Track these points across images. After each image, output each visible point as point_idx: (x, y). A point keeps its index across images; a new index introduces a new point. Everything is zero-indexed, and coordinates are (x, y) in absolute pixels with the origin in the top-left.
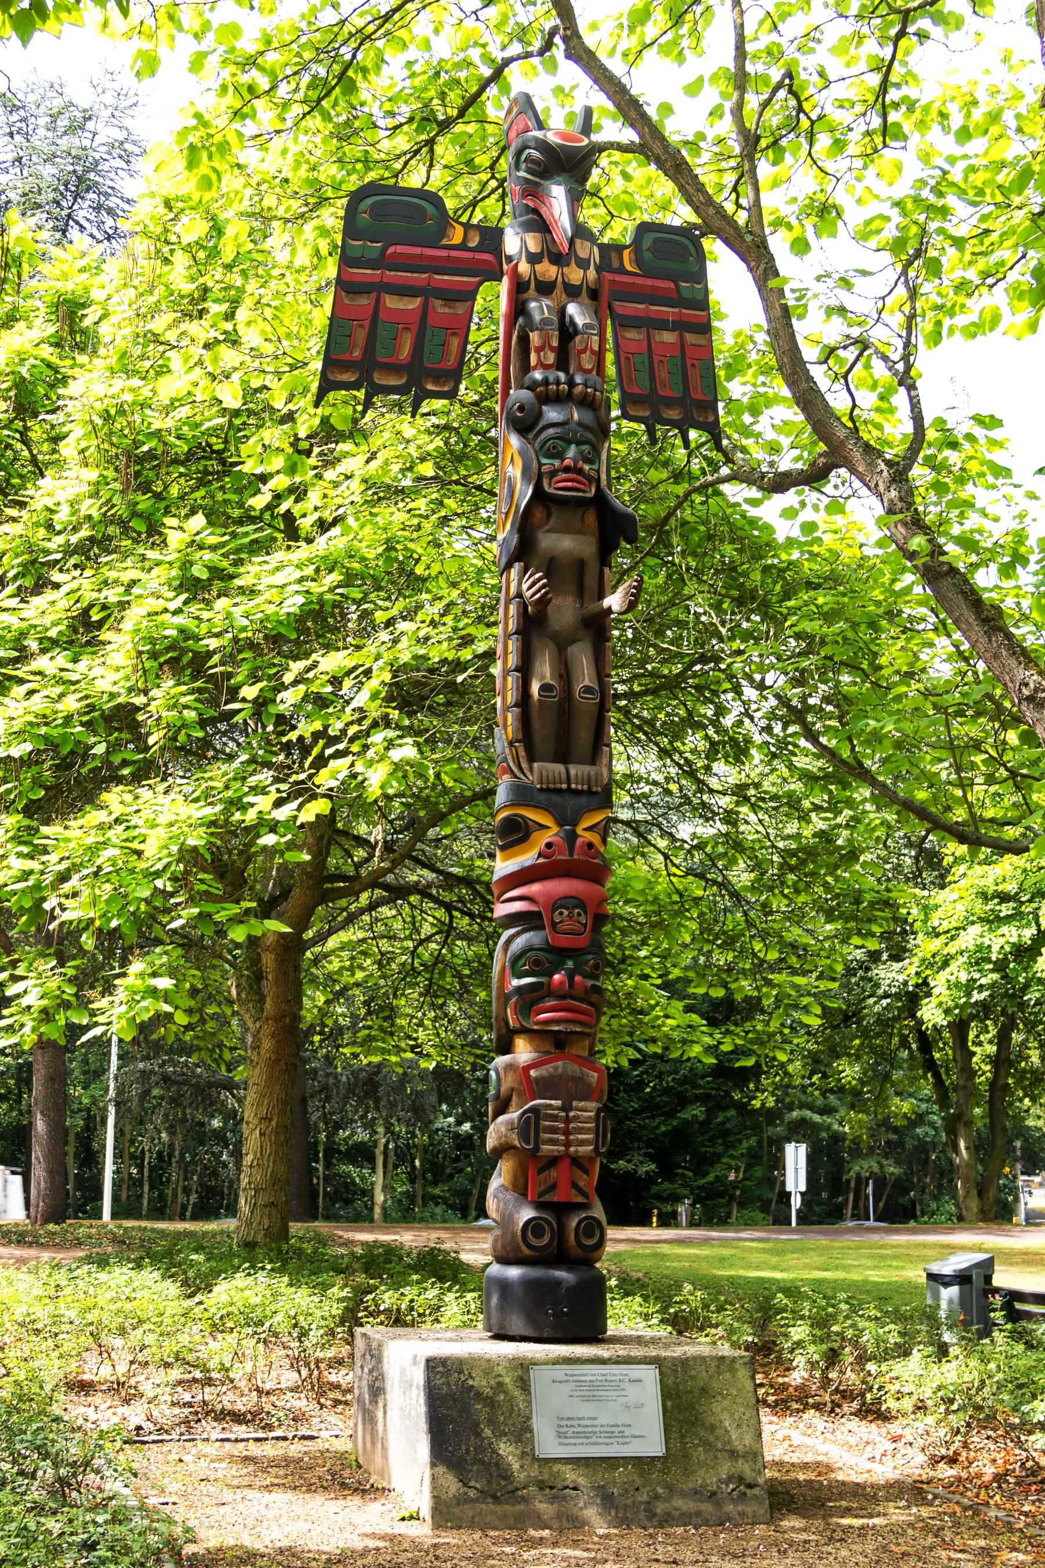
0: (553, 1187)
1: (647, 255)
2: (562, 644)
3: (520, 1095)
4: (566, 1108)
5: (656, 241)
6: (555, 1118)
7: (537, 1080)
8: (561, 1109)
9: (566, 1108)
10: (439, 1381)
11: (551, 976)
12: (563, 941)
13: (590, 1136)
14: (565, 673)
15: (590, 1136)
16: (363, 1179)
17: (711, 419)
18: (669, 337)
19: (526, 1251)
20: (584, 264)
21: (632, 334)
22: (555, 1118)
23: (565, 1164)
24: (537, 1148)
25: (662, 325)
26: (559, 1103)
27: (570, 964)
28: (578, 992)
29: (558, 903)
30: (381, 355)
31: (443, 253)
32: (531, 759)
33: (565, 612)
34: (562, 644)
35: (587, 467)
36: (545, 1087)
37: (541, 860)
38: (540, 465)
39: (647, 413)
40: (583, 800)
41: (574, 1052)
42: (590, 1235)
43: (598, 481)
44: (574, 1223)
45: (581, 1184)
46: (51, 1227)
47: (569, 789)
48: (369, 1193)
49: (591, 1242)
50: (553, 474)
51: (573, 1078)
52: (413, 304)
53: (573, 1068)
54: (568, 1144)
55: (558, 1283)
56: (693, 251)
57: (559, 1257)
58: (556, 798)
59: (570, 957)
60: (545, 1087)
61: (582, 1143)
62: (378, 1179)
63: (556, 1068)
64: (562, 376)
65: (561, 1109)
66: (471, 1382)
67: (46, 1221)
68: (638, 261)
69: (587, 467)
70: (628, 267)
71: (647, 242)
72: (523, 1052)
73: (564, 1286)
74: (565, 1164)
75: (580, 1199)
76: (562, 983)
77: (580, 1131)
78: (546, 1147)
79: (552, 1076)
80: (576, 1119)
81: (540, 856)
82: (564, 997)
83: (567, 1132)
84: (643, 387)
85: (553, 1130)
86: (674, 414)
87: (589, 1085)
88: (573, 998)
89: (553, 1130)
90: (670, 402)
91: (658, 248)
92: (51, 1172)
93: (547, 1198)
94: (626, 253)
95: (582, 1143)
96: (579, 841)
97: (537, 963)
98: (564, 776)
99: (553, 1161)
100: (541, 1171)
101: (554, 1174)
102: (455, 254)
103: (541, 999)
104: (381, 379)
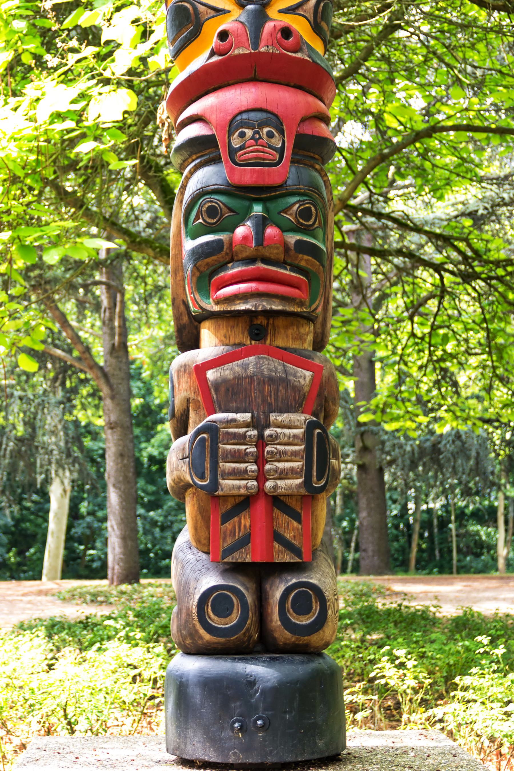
0: (244, 542)
3: (197, 408)
4: (259, 424)
6: (241, 439)
7: (217, 385)
8: (253, 424)
9: (259, 424)
11: (233, 231)
12: (247, 176)
13: (297, 465)
15: (297, 465)
16: (488, 535)
19: (207, 637)
22: (241, 439)
23: (261, 507)
24: (215, 484)
26: (247, 416)
27: (258, 209)
28: (277, 253)
29: (234, 123)
36: (228, 395)
37: (216, 59)
41: (280, 342)
42: (303, 609)
44: (278, 594)
45: (289, 535)
46: (125, 587)
48: (492, 547)
49: (305, 621)
51: (271, 380)
53: (272, 366)
54: (261, 477)
55: (251, 682)
57: (260, 644)
59: (257, 200)
60: (228, 395)
61: (284, 475)
62: (501, 535)
63: (245, 367)
65: (253, 424)
67: (122, 581)
72: (211, 343)
73: (260, 686)
74: (261, 507)
75: (287, 558)
76: (245, 238)
77: (281, 457)
78: (227, 484)
79: (239, 378)
80: (274, 439)
81: (213, 53)
82: (252, 260)
83: (260, 460)
85: (239, 457)
87: (298, 390)
88: (266, 261)
89: (239, 457)
92: (124, 538)
93: (237, 557)
95: (284, 475)
96: (269, 26)
97: (212, 212)
99: (244, 503)
100: (227, 517)
101: (245, 520)
103: (223, 266)
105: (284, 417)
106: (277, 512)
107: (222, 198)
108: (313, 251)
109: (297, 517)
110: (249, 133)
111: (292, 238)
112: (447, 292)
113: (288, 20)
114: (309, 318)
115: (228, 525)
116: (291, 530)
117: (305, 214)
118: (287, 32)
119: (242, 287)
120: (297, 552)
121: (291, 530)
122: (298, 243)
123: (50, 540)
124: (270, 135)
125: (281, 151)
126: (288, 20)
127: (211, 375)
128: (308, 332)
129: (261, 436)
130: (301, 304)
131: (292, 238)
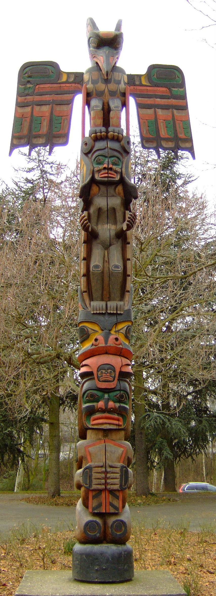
2: (107, 247)
14: (106, 261)
27: (106, 396)
32: (91, 299)
33: (106, 230)
34: (107, 247)
38: (94, 168)
40: (114, 319)
50: (99, 171)
58: (101, 318)
64: (103, 129)
83: (106, 472)
98: (104, 307)
104: (35, 141)
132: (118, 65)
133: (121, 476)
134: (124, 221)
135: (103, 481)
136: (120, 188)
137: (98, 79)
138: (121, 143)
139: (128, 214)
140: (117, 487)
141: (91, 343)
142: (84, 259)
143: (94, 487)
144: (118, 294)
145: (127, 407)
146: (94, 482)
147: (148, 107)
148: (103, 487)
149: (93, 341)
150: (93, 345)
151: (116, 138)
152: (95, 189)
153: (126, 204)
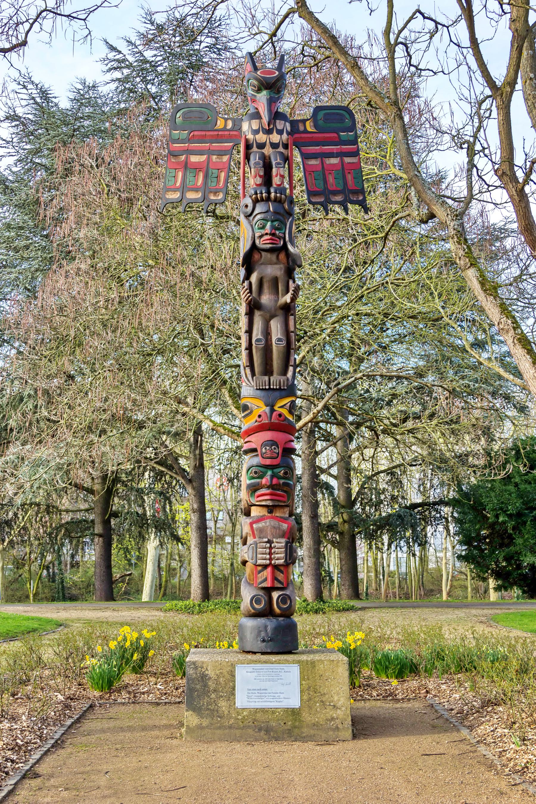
0: (266, 580)
1: (321, 122)
5: (325, 114)
10: (32, 587)
17: (361, 198)
18: (334, 161)
20: (280, 132)
21: (313, 162)
25: (331, 155)
30: (189, 184)
31: (216, 133)
35: (277, 232)
39: (322, 200)
40: (277, 394)
42: (285, 603)
43: (284, 239)
45: (279, 578)
47: (270, 389)
52: (204, 158)
54: (270, 559)
56: (347, 116)
66: (207, 672)
68: (316, 126)
69: (277, 232)
70: (309, 129)
71: (321, 114)
75: (280, 585)
84: (320, 186)
86: (339, 198)
90: (335, 193)
91: (327, 118)
94: (308, 123)
97: (256, 473)
102: (220, 133)
105: (278, 540)
106: (276, 571)
107: (260, 468)
108: (288, 485)
109: (282, 572)
110: (268, 448)
111: (282, 481)
112: (499, 297)
113: (281, 410)
114: (287, 506)
115: (260, 575)
116: (281, 576)
117: (286, 473)
118: (280, 415)
119: (268, 242)
120: (283, 584)
121: (281, 576)
122: (283, 483)
123: (144, 592)
124: (275, 449)
125: (278, 453)
126: (281, 410)
127: (254, 526)
128: (287, 510)
129: (271, 546)
130: (284, 502)
131: (282, 481)
132: (279, 110)
133: (286, 551)
134: (287, 291)
135: (268, 556)
136: (282, 256)
137: (299, 662)
138: (252, 515)
139: (292, 286)
140: (282, 562)
141: (254, 420)
142: (246, 332)
143: (259, 562)
144: (265, 280)
145: (292, 483)
146: (259, 556)
147: (314, 156)
148: (268, 562)
149: (256, 418)
150: (256, 421)
151: (278, 200)
152: (256, 256)
153: (290, 273)
